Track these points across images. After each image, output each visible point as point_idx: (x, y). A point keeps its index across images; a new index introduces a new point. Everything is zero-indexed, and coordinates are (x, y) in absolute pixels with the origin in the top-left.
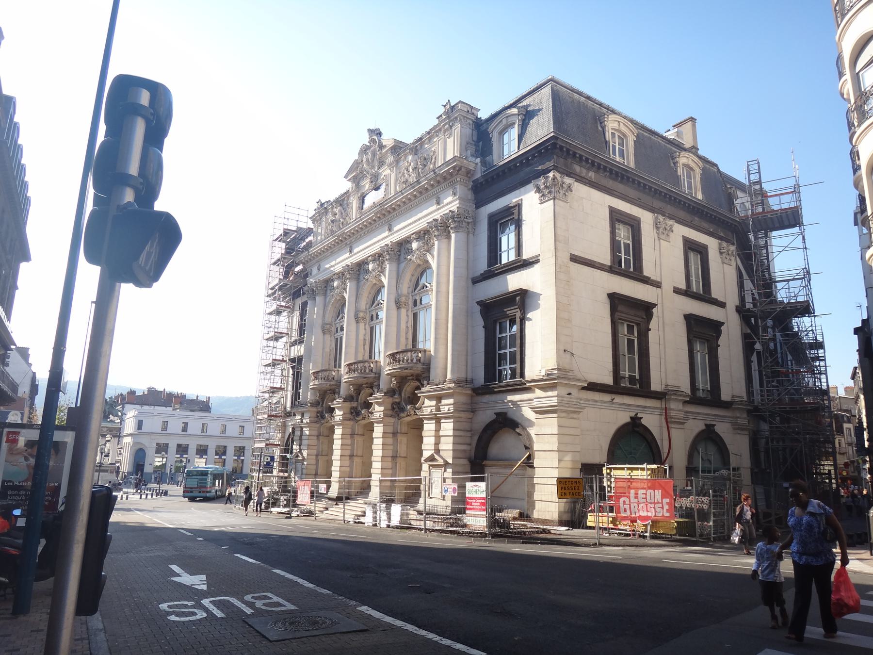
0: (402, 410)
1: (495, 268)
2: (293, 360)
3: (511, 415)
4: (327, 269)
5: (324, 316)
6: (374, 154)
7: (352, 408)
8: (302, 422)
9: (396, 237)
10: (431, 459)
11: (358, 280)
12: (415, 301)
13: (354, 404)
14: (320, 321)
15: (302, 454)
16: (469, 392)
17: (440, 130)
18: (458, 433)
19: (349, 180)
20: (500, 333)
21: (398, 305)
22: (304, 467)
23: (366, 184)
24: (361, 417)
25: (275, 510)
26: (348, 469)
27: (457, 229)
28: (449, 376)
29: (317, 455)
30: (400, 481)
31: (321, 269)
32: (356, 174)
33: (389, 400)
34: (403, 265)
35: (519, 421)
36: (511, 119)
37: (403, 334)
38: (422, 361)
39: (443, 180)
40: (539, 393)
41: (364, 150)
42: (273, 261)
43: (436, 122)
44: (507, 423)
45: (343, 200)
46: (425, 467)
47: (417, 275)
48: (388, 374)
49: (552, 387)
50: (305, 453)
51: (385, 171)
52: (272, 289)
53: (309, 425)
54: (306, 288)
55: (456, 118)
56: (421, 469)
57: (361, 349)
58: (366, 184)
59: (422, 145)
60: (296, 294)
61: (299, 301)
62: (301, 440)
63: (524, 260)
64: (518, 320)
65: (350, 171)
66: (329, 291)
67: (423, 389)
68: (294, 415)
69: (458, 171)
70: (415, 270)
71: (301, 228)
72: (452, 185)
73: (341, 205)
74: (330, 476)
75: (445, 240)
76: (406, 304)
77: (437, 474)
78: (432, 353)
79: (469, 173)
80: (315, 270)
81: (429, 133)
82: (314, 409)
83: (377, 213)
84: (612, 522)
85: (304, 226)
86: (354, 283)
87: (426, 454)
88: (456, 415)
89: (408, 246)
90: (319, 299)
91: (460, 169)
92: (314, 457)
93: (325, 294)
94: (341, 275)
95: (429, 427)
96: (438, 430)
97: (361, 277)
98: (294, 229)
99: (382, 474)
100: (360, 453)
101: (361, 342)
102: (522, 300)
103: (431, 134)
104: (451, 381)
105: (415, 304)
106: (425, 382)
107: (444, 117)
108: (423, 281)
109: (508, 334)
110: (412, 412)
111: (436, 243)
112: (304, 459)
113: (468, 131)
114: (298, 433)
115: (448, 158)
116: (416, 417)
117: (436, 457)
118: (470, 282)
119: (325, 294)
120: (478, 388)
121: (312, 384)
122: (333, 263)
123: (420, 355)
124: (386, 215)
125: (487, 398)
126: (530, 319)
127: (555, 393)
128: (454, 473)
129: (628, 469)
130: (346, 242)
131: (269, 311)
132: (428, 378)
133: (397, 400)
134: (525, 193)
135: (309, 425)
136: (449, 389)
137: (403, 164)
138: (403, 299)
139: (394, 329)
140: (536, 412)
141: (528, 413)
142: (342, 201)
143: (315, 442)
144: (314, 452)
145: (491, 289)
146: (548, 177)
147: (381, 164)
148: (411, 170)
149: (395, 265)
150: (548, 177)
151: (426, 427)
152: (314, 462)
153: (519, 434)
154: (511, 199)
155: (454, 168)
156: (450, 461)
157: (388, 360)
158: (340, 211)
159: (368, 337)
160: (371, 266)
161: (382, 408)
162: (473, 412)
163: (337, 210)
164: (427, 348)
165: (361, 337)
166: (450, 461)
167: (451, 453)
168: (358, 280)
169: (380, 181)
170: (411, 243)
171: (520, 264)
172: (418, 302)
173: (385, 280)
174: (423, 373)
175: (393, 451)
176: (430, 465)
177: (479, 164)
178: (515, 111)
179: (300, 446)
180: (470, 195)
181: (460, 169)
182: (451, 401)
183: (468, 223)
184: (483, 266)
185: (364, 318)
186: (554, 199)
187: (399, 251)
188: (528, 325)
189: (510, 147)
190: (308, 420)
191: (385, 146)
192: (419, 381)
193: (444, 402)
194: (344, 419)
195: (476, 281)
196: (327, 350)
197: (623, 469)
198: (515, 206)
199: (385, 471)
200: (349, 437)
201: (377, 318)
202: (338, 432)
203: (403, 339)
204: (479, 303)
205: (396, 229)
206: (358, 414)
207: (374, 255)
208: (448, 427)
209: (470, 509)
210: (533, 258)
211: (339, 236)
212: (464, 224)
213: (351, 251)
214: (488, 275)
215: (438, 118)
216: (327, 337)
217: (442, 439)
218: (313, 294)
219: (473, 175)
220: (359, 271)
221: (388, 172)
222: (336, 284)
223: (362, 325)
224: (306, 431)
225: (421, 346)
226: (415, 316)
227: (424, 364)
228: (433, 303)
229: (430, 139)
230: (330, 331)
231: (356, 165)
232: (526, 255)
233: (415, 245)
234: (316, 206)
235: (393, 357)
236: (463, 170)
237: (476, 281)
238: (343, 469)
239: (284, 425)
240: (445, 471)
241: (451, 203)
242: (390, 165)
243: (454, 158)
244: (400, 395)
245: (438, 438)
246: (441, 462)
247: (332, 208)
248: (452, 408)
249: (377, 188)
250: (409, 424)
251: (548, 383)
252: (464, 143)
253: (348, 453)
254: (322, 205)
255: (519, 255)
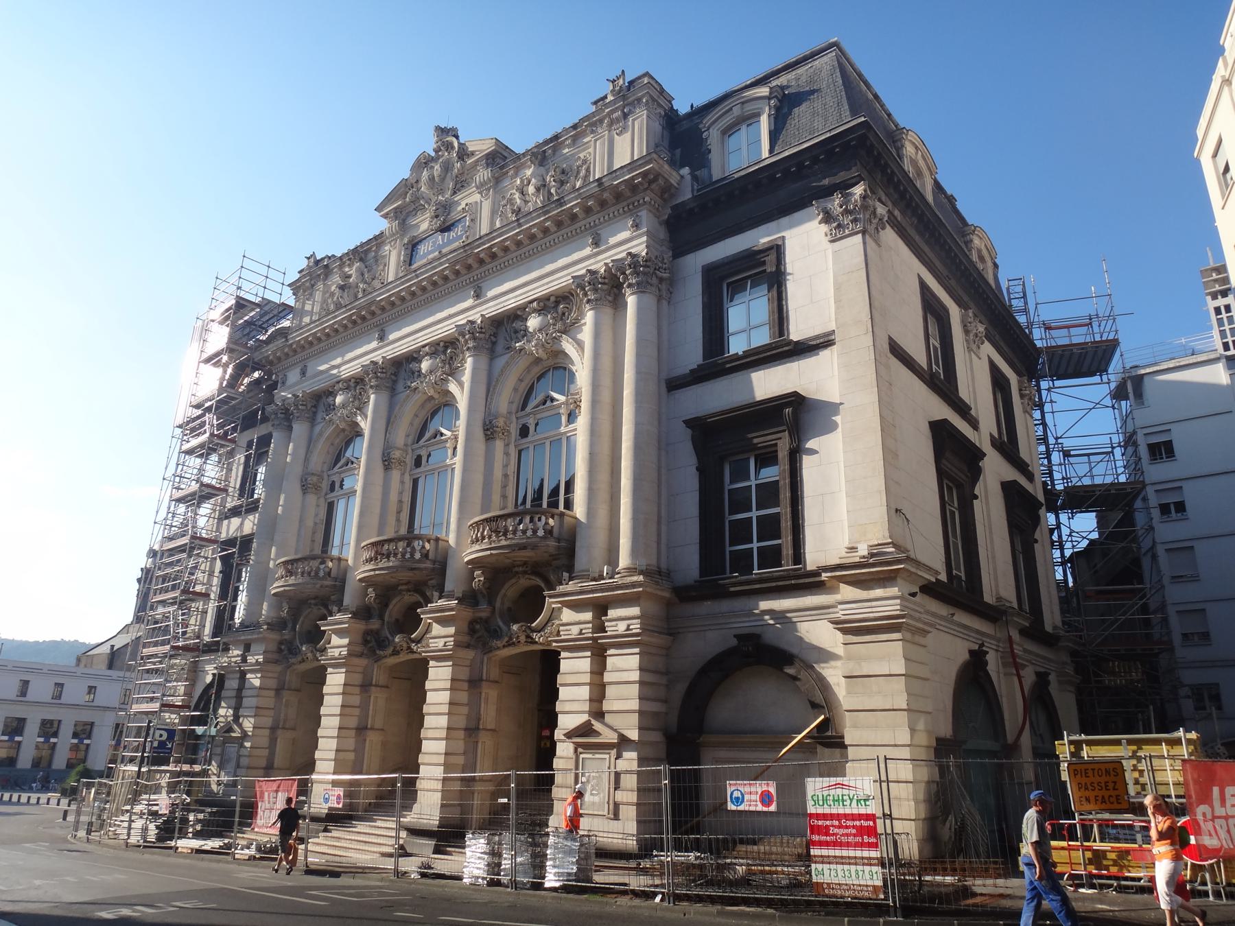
0: (496, 634)
1: (717, 363)
2: (230, 542)
3: (769, 638)
4: (322, 372)
5: (307, 460)
6: (447, 167)
7: (367, 633)
8: (244, 660)
9: (492, 309)
10: (585, 730)
11: (393, 392)
12: (333, 484)
13: (375, 624)
14: (298, 470)
15: (240, 726)
16: (667, 594)
17: (601, 121)
18: (650, 678)
19: (385, 216)
20: (731, 482)
21: (387, 463)
22: (243, 752)
23: (423, 223)
24: (390, 650)
25: (186, 844)
26: (351, 756)
27: (640, 289)
28: (624, 561)
29: (273, 729)
30: (482, 779)
31: (309, 372)
32: (401, 204)
33: (361, 626)
34: (501, 362)
35: (795, 651)
36: (750, 108)
37: (497, 488)
38: (431, 556)
39: (614, 199)
40: (847, 592)
41: (424, 162)
42: (205, 356)
43: (298, 276)
44: (776, 657)
45: (369, 250)
46: (564, 749)
47: (423, 415)
48: (360, 580)
49: (885, 579)
50: (248, 724)
51: (470, 197)
52: (197, 406)
53: (260, 668)
54: (270, 409)
55: (639, 100)
56: (551, 751)
57: (391, 520)
58: (423, 223)
59: (555, 149)
60: (249, 422)
61: (254, 435)
62: (239, 697)
63: (797, 343)
64: (783, 454)
65: (389, 199)
66: (320, 415)
67: (561, 589)
68: (226, 649)
69: (650, 182)
70: (528, 369)
71: (269, 302)
72: (632, 210)
73: (361, 260)
74: (310, 766)
75: (608, 311)
76: (506, 432)
77: (598, 767)
78: (350, 562)
79: (667, 191)
80: (293, 376)
81: (575, 127)
82: (275, 636)
83: (456, 262)
84: (1091, 862)
85: (276, 299)
86: (385, 396)
87: (567, 722)
88: (646, 638)
89: (414, 365)
90: (299, 428)
91: (655, 180)
92: (267, 732)
93: (312, 421)
94: (356, 384)
95: (574, 667)
96: (599, 668)
97: (400, 387)
98: (258, 300)
99: (448, 767)
100: (378, 725)
101: (393, 507)
102: (796, 417)
103: (577, 131)
104: (631, 571)
105: (524, 432)
106: (335, 609)
107: (610, 98)
108: (348, 454)
109: (753, 482)
110: (523, 638)
111: (372, 397)
112: (245, 735)
113: (657, 126)
114: (232, 684)
115: (616, 166)
116: (315, 664)
117: (597, 726)
118: (664, 388)
119: (312, 421)
120: (688, 588)
121: (276, 587)
122: (339, 361)
123: (427, 546)
124: (476, 268)
125: (707, 607)
126: (813, 452)
127: (894, 591)
128: (642, 761)
129: (1130, 742)
130: (374, 318)
131: (186, 447)
132: (570, 568)
133: (484, 615)
134: (791, 227)
135: (260, 668)
136: (633, 585)
137: (511, 187)
138: (397, 454)
139: (478, 478)
140: (845, 631)
141: (818, 633)
142: (365, 254)
143: (270, 702)
144: (268, 721)
145: (717, 397)
146: (851, 194)
147: (461, 184)
148: (531, 189)
149: (484, 360)
150: (851, 194)
151: (565, 665)
152: (264, 741)
153: (795, 678)
154: (761, 237)
155: (644, 175)
156: (634, 735)
157: (366, 555)
158: (358, 269)
159: (407, 498)
160: (425, 365)
161: (346, 641)
162: (670, 634)
163: (353, 271)
164: (343, 556)
165: (394, 497)
166: (634, 735)
167: (634, 719)
168: (393, 392)
169: (455, 215)
170: (420, 362)
171: (785, 350)
172: (337, 485)
173: (365, 425)
174: (555, 557)
175: (468, 717)
176: (577, 745)
177: (689, 178)
178: (764, 91)
179: (237, 709)
180: (662, 234)
181: (655, 180)
182: (635, 611)
183: (661, 280)
184: (692, 354)
185: (401, 462)
186: (864, 232)
187: (395, 374)
188: (807, 462)
189: (751, 148)
190: (261, 658)
191: (473, 154)
192: (326, 607)
193: (612, 613)
194: (350, 654)
195: (675, 384)
196: (310, 523)
197: (1118, 743)
198: (770, 248)
199: (453, 759)
200: (357, 690)
201: (341, 486)
202: (335, 680)
203: (496, 498)
204: (690, 423)
205: (392, 337)
206: (294, 651)
207: (436, 344)
208: (625, 666)
209: (821, 844)
210: (817, 337)
211: (360, 309)
212: (655, 281)
213: (381, 338)
214: (701, 375)
215: (595, 103)
216: (312, 499)
217: (610, 691)
218: (286, 418)
219: (673, 196)
220: (395, 374)
221: (476, 197)
222: (339, 399)
223: (395, 475)
224: (255, 680)
225: (335, 552)
226: (331, 507)
227: (559, 540)
228: (359, 487)
229: (575, 139)
230: (317, 488)
231: (404, 187)
232: (797, 332)
233: (533, 323)
234: (304, 264)
235: (379, 550)
236: (661, 181)
237: (675, 384)
238: (342, 755)
239: (194, 671)
240: (619, 757)
241: (628, 241)
242: (482, 185)
243: (632, 165)
244: (381, 617)
245: (599, 691)
246: (610, 737)
247: (341, 266)
248: (636, 626)
249: (445, 229)
250: (393, 668)
251: (868, 572)
252: (652, 144)
253: (353, 722)
254: (317, 262)
255: (781, 333)
